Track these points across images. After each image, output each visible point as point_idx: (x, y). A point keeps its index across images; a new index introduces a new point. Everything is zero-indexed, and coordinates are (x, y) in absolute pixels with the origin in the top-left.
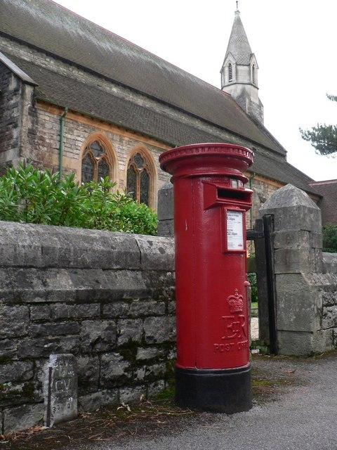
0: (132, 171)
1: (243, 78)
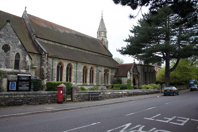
0: (67, 68)
1: (103, 35)
